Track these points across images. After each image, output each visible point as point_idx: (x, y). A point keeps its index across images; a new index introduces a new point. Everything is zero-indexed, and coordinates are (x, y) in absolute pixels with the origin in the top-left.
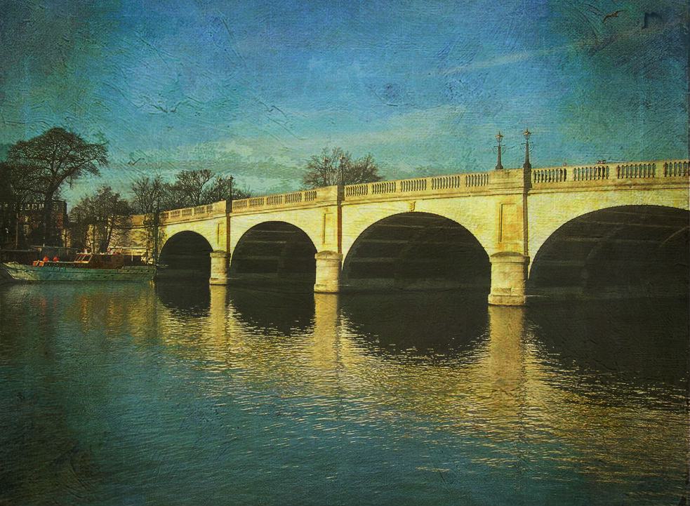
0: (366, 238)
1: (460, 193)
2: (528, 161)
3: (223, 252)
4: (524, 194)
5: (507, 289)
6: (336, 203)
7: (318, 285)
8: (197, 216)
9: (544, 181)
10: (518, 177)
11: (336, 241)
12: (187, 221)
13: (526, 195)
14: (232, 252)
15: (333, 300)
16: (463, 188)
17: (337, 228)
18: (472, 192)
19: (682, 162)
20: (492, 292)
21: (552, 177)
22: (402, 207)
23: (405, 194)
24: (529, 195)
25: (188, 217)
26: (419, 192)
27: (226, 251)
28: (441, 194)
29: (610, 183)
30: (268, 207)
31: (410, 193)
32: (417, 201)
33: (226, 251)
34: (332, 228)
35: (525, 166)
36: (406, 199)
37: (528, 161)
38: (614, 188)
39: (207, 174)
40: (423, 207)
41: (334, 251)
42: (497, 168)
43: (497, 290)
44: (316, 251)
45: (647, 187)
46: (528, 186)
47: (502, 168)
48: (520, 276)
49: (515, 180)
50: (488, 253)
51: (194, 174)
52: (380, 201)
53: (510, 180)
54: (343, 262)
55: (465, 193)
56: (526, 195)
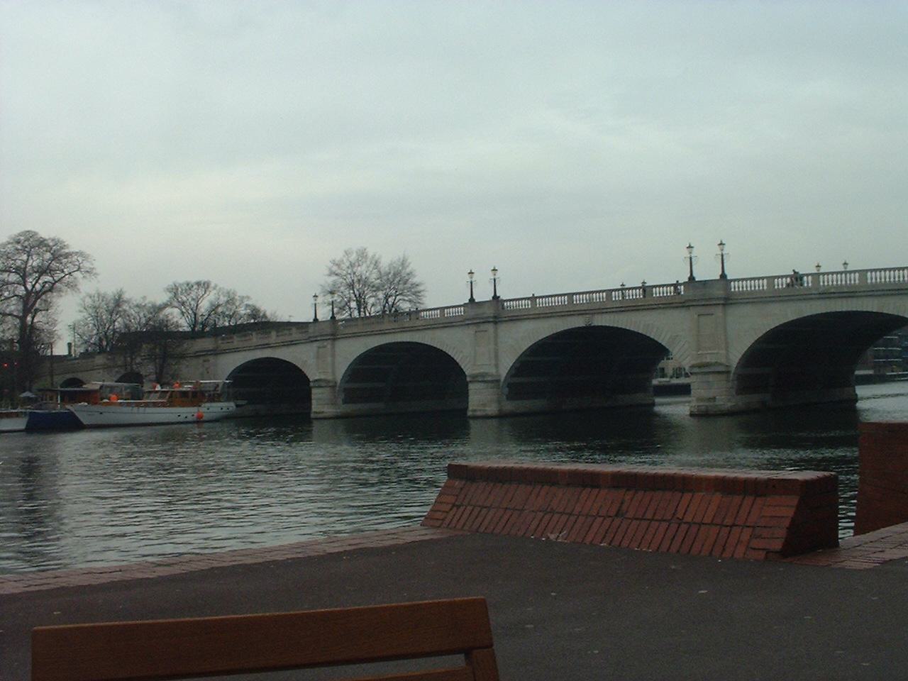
39: (205, 286)
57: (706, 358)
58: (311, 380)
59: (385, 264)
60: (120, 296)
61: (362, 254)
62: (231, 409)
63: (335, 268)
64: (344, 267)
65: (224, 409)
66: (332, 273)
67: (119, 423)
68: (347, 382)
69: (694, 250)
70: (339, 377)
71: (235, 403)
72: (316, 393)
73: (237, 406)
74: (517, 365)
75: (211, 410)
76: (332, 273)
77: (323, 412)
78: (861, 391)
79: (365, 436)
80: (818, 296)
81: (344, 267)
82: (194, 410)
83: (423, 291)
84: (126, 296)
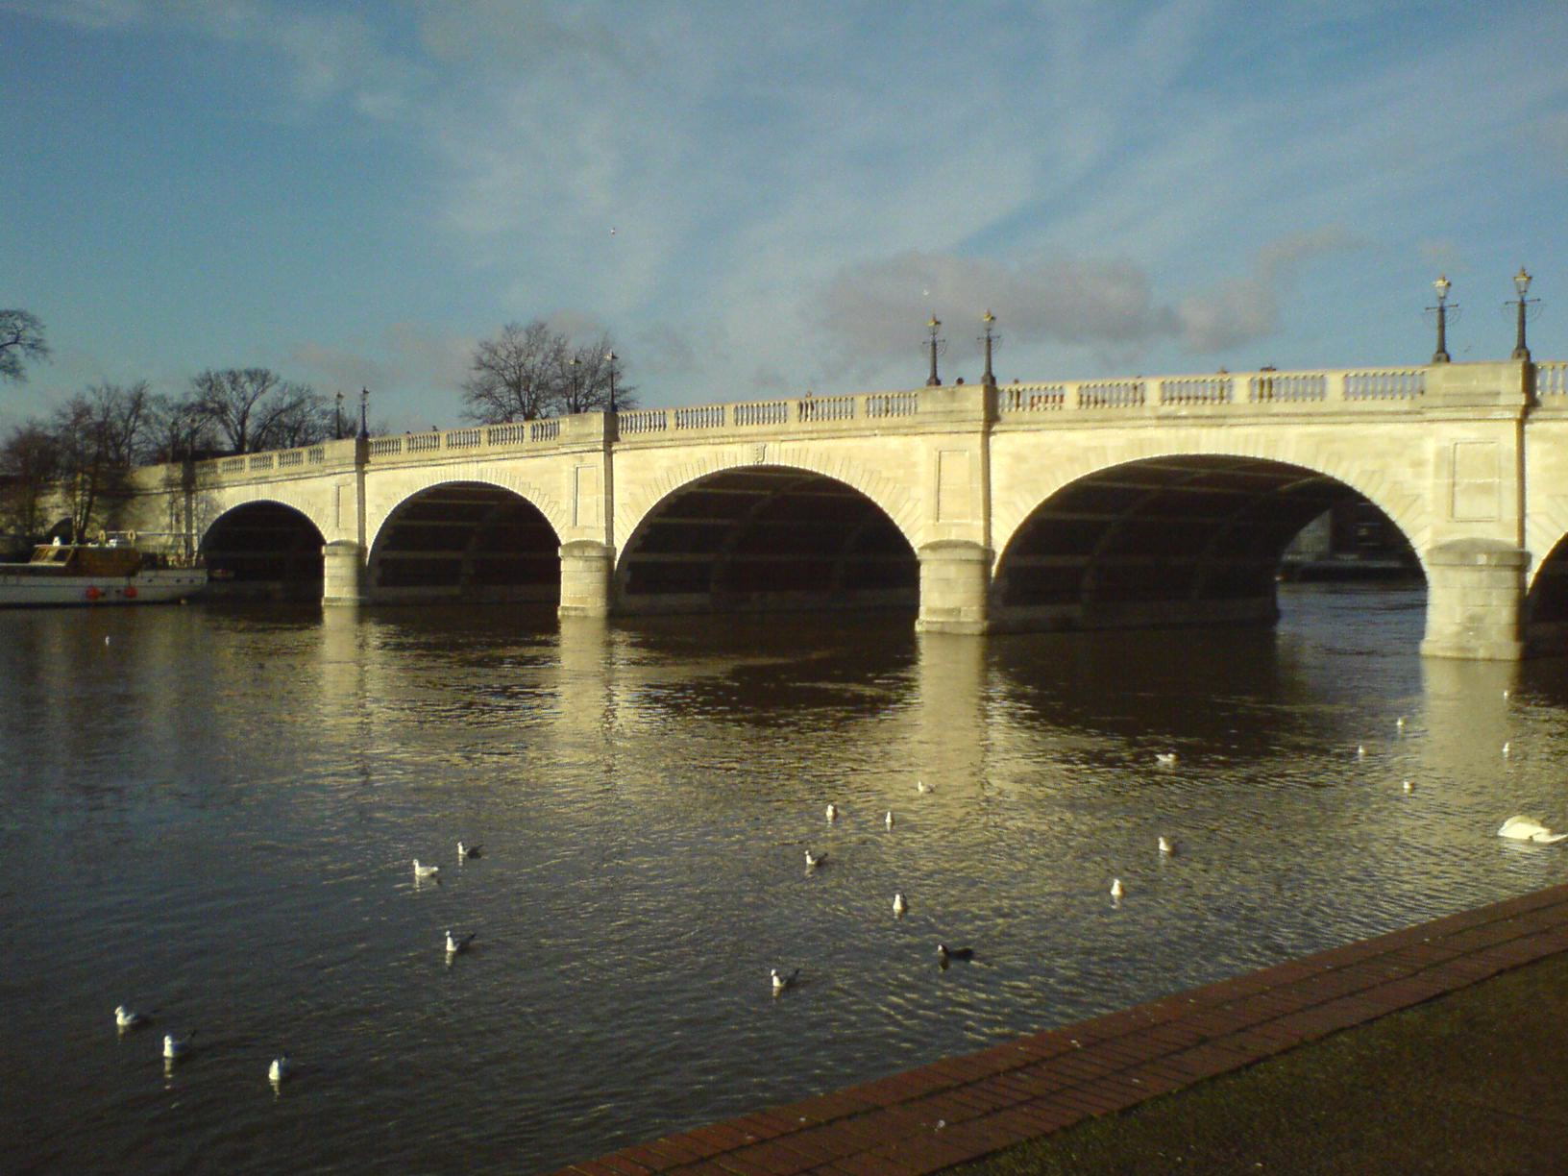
0: (399, 518)
1: (856, 429)
2: (989, 372)
3: (969, 545)
4: (983, 432)
5: (953, 610)
6: (601, 447)
7: (565, 609)
8: (287, 469)
9: (647, 430)
10: (974, 399)
11: (603, 524)
12: (264, 480)
13: (987, 433)
14: (369, 545)
15: (969, 656)
16: (793, 424)
17: (602, 496)
18: (878, 428)
19: (1123, 383)
20: (923, 616)
21: (657, 424)
22: (735, 455)
23: (745, 429)
24: (994, 433)
25: (263, 473)
26: (772, 428)
27: (981, 543)
28: (817, 432)
29: (1148, 413)
30: (450, 453)
31: (754, 428)
32: (770, 445)
33: (981, 543)
34: (592, 501)
35: (984, 380)
36: (746, 439)
37: (989, 372)
38: (1154, 422)
39: (260, 378)
40: (783, 453)
41: (599, 540)
42: (929, 383)
43: (932, 611)
44: (323, 542)
45: (1216, 420)
46: (992, 417)
47: (938, 383)
48: (1513, 593)
49: (969, 405)
50: (912, 544)
51: (234, 377)
52: (687, 442)
53: (955, 406)
54: (616, 563)
55: (867, 429)
56: (987, 433)
57: (950, 532)
58: (563, 542)
59: (573, 347)
60: (141, 395)
61: (537, 331)
62: (197, 582)
63: (485, 357)
64: (503, 353)
65: (185, 582)
66: (482, 365)
67: (45, 601)
68: (385, 548)
69: (344, 400)
70: (1000, 542)
71: (208, 573)
72: (568, 567)
73: (211, 579)
74: (646, 531)
75: (156, 582)
76: (482, 365)
77: (340, 599)
78: (1285, 599)
79: (1079, 727)
80: (755, 438)
81: (503, 353)
82: (121, 582)
83: (631, 388)
84: (153, 391)
